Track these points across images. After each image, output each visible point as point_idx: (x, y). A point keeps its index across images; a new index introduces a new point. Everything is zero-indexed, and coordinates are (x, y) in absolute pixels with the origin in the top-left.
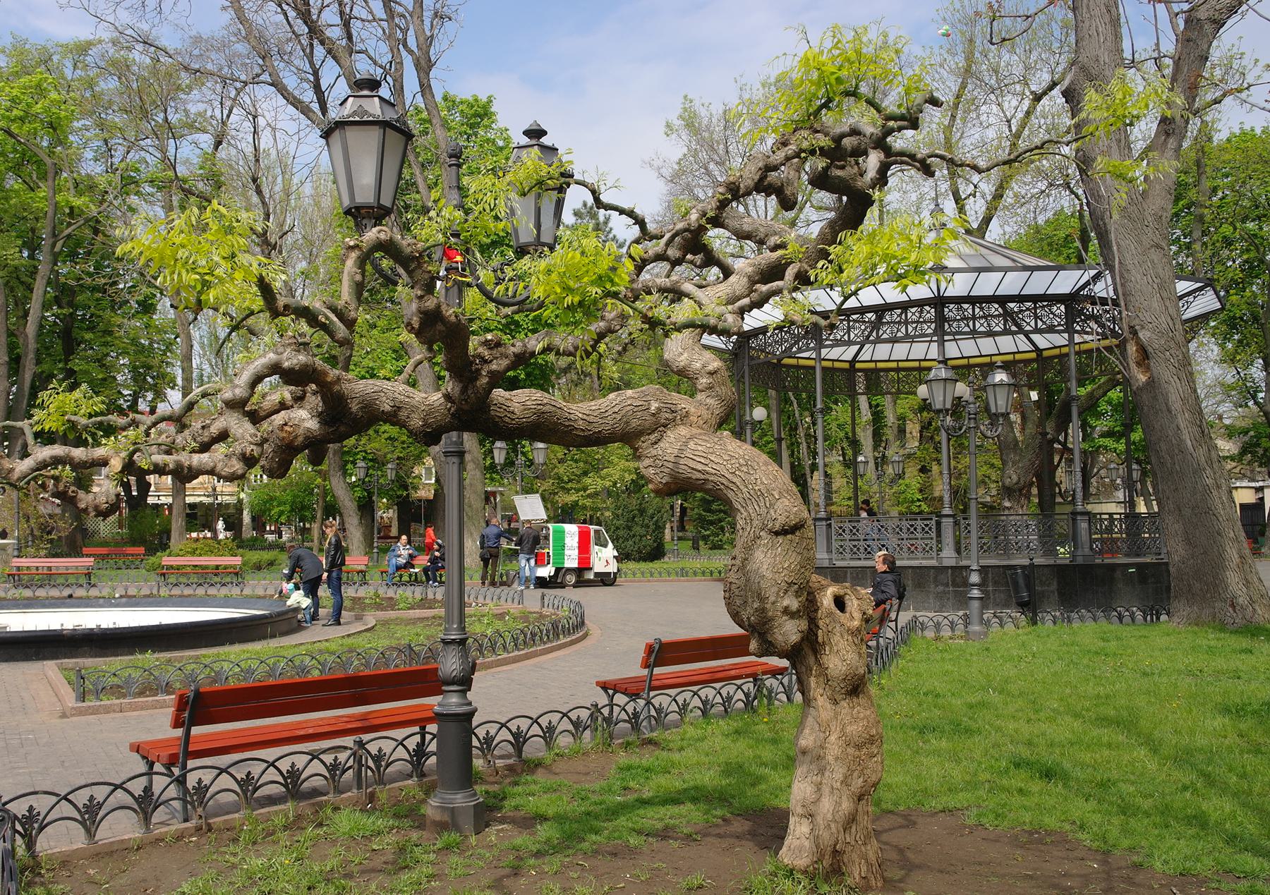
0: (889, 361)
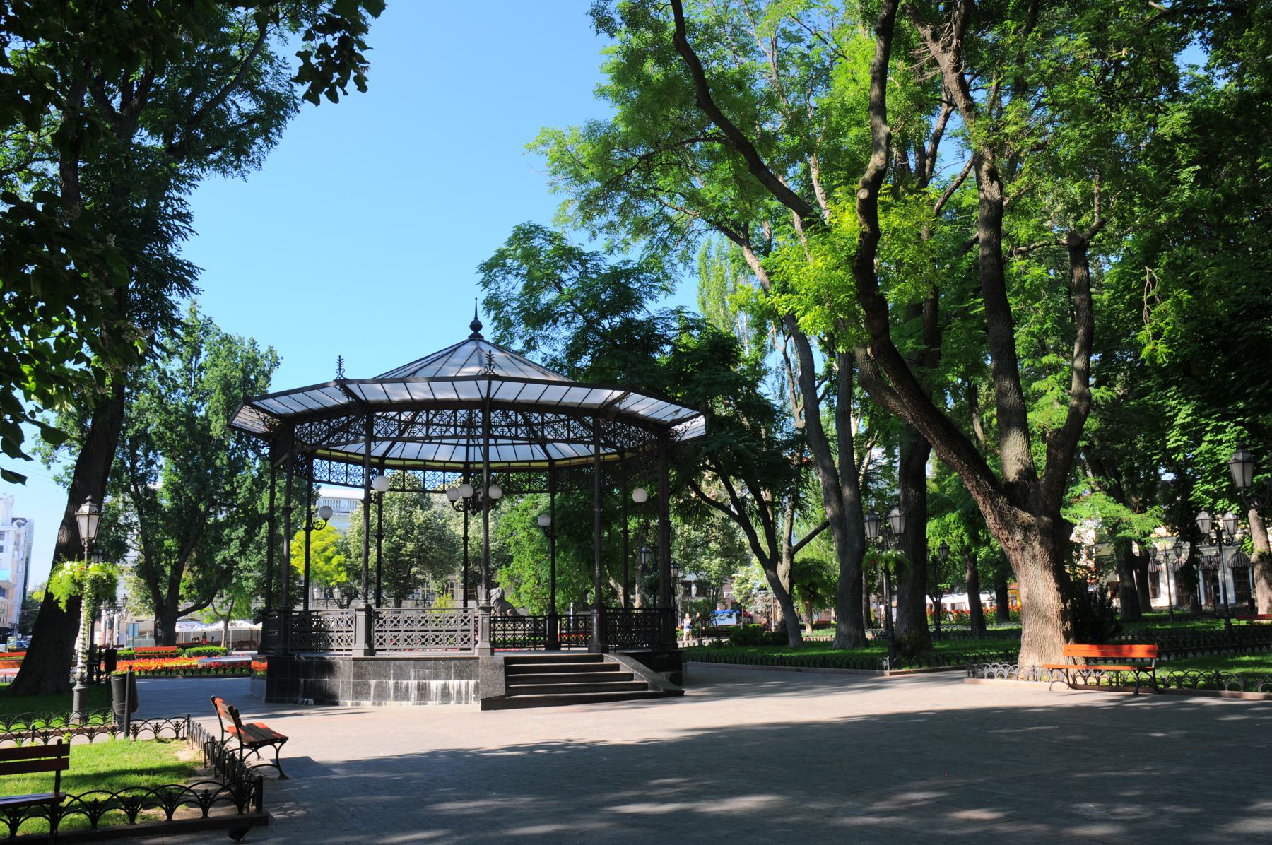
0: (416, 460)
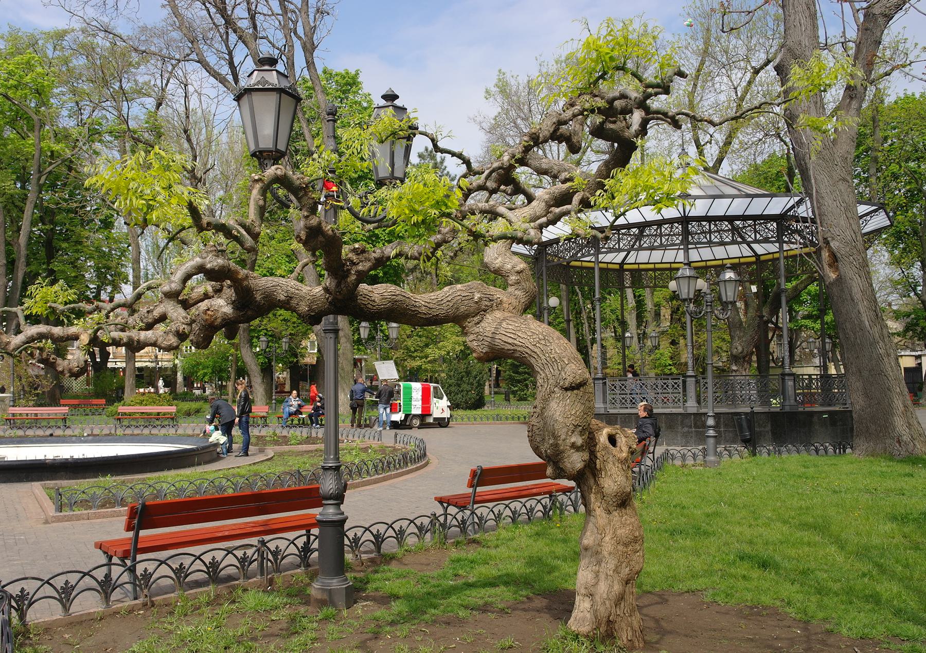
0: (648, 263)
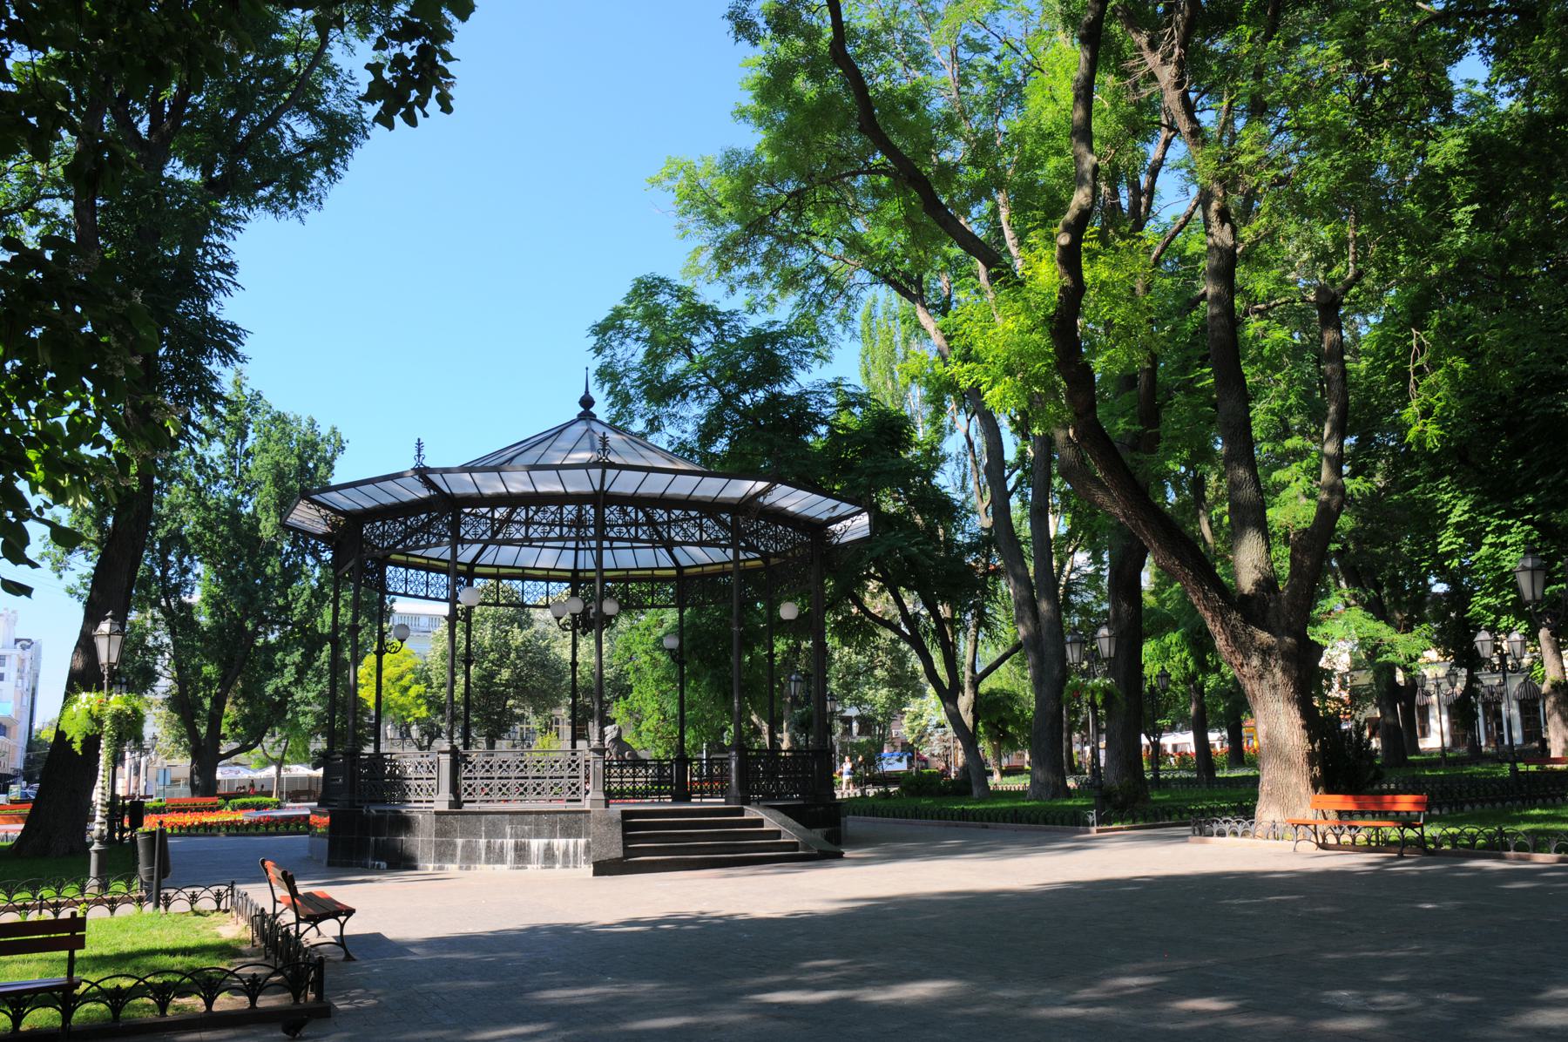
0: (513, 567)
